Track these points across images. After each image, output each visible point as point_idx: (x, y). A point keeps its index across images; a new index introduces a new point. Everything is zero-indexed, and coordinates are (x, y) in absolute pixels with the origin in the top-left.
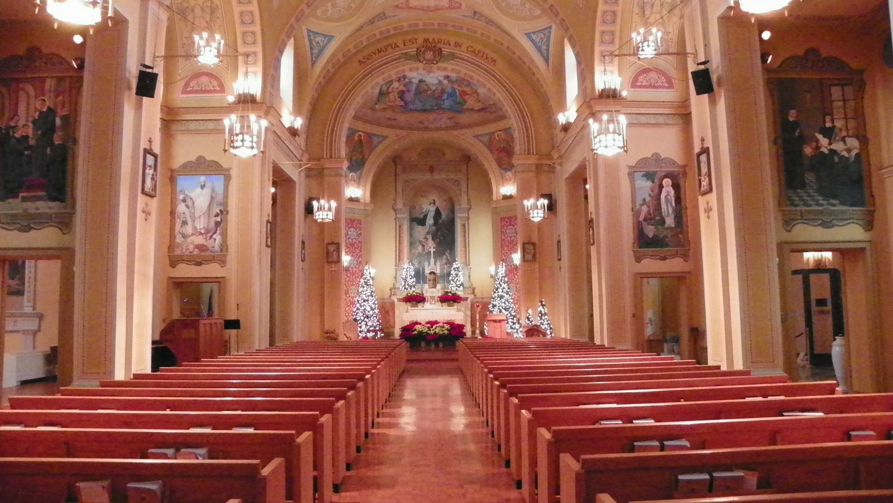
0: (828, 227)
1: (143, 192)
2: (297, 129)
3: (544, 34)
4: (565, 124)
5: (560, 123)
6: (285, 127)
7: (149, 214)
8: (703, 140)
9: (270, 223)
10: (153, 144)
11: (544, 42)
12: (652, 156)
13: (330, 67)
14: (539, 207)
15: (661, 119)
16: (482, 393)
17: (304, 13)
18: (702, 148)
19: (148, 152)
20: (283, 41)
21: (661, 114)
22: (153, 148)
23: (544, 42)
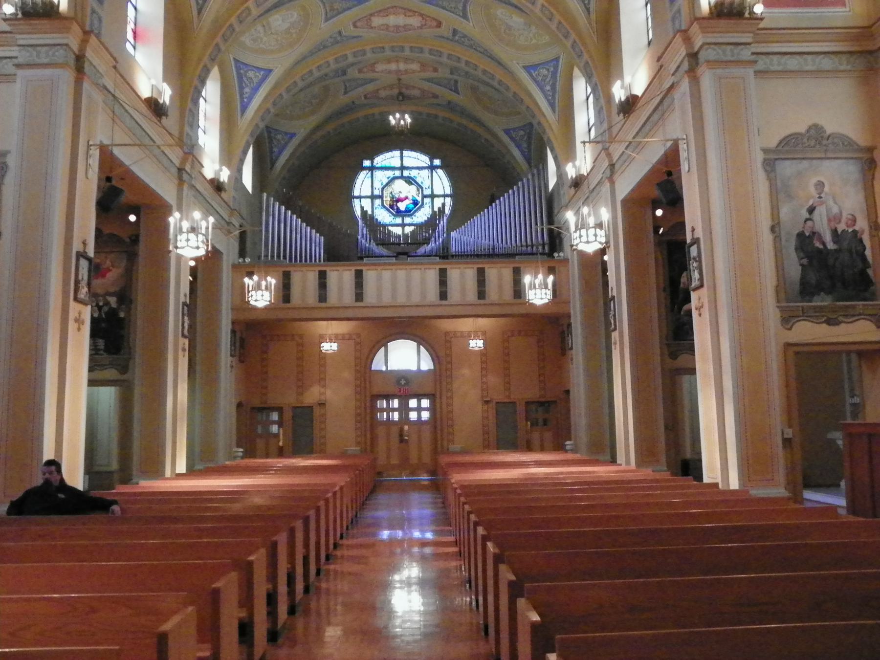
0: (833, 325)
1: (76, 299)
2: (223, 183)
3: (548, 70)
4: (576, 177)
5: (569, 177)
6: (206, 179)
7: (83, 323)
8: (693, 230)
9: (187, 306)
10: (87, 247)
11: (548, 80)
12: (808, 131)
13: (269, 105)
14: (537, 287)
15: (827, 63)
16: (464, 524)
17: (234, 30)
18: (693, 238)
19: (81, 255)
20: (205, 66)
21: (828, 53)
22: (87, 251)
23: (548, 80)
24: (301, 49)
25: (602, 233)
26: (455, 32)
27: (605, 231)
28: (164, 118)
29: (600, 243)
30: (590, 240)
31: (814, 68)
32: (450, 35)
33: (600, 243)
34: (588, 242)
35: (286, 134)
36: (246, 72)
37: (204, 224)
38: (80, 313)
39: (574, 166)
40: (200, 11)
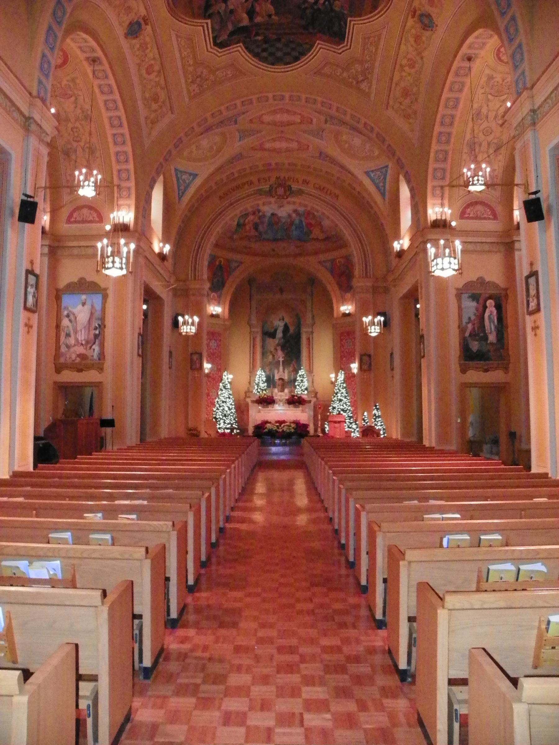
4: (400, 251)
5: (395, 250)
14: (376, 324)
15: (487, 247)
24: (218, 162)
25: (456, 261)
26: (321, 154)
27: (458, 260)
28: (165, 261)
29: (454, 270)
30: (444, 268)
31: (480, 249)
32: (318, 155)
33: (454, 270)
34: (443, 269)
35: (190, 174)
36: (182, 176)
37: (125, 250)
38: (29, 319)
39: (399, 243)
40: (180, 199)
